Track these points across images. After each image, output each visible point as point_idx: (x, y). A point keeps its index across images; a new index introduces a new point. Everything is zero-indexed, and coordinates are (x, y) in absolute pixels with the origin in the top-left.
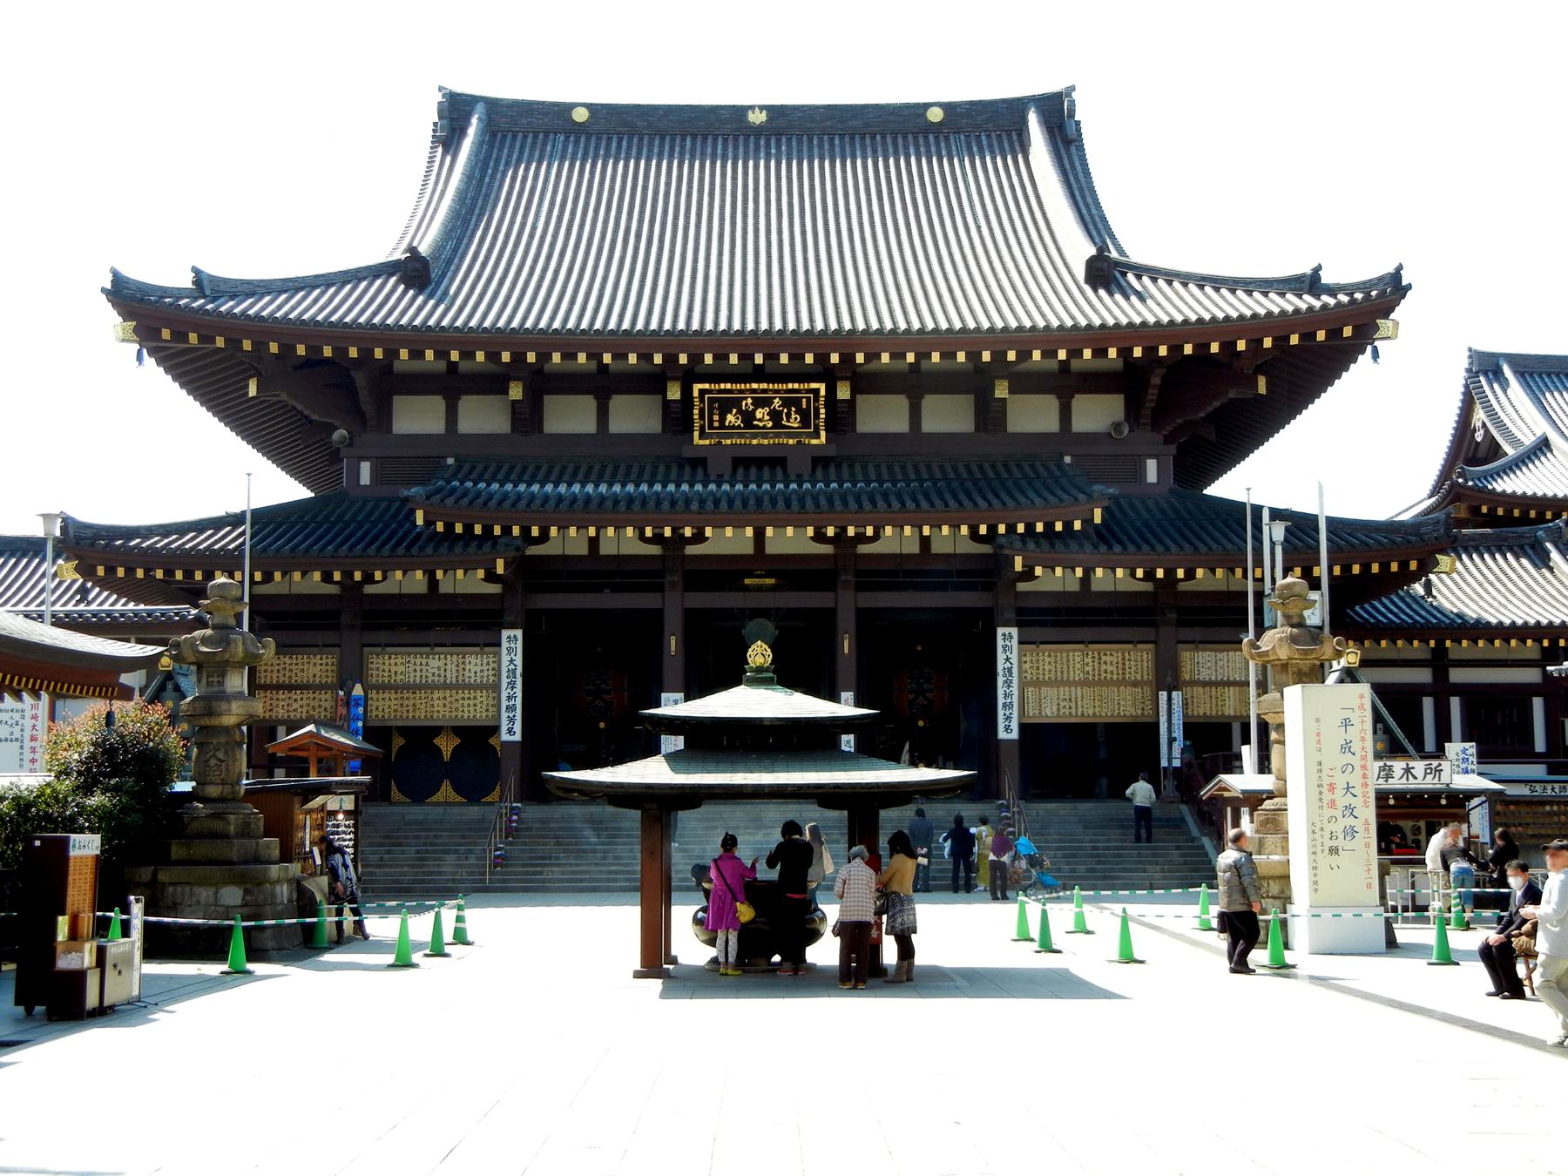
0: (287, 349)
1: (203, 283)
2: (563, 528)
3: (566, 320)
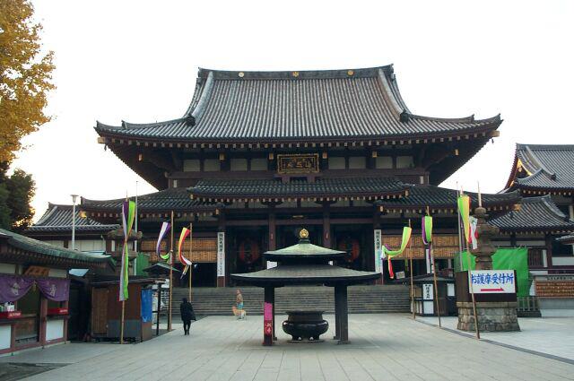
2: (286, 199)
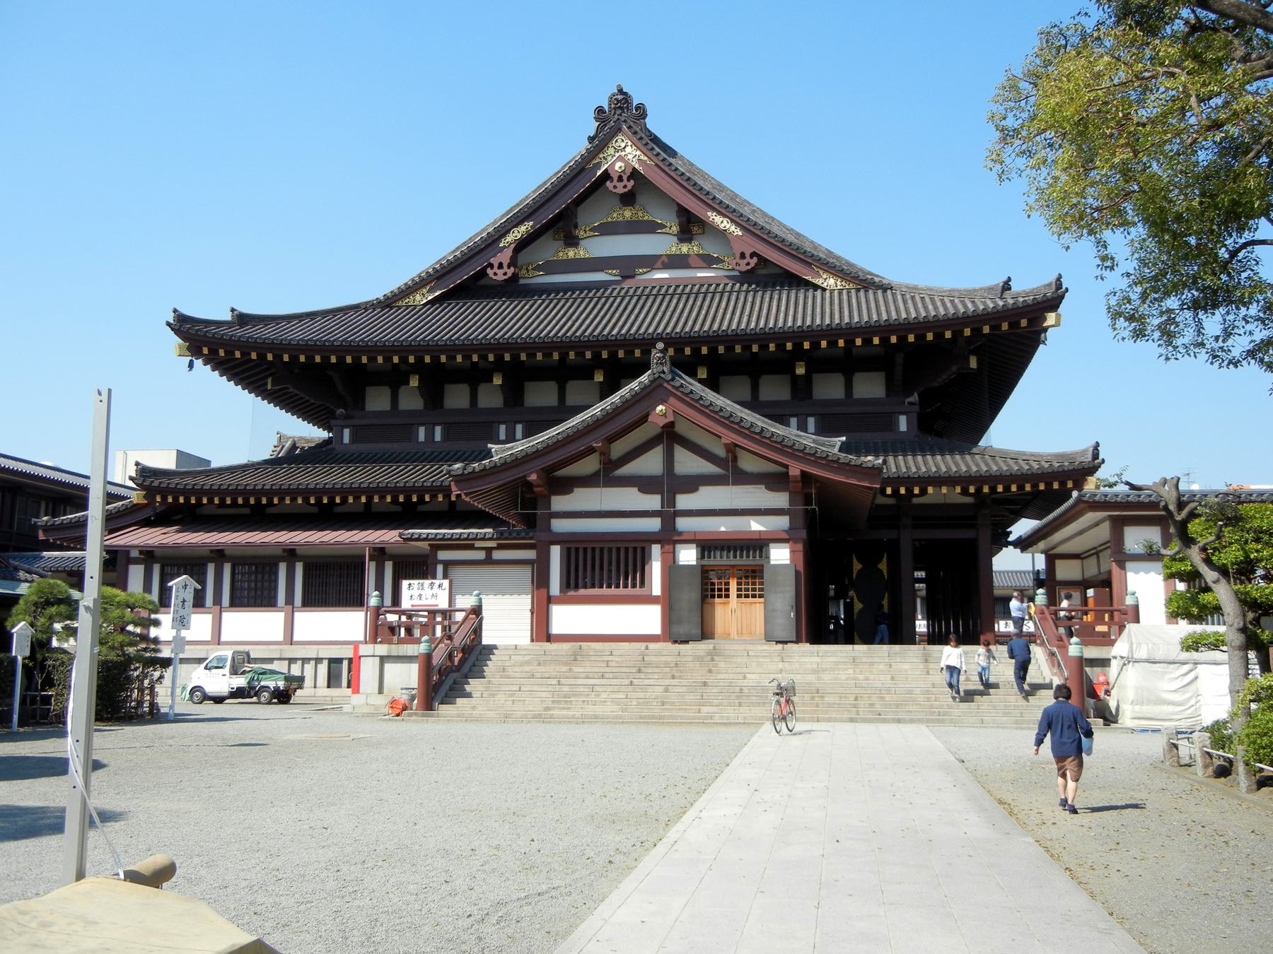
0: (294, 358)
1: (243, 319)
3: (739, 323)
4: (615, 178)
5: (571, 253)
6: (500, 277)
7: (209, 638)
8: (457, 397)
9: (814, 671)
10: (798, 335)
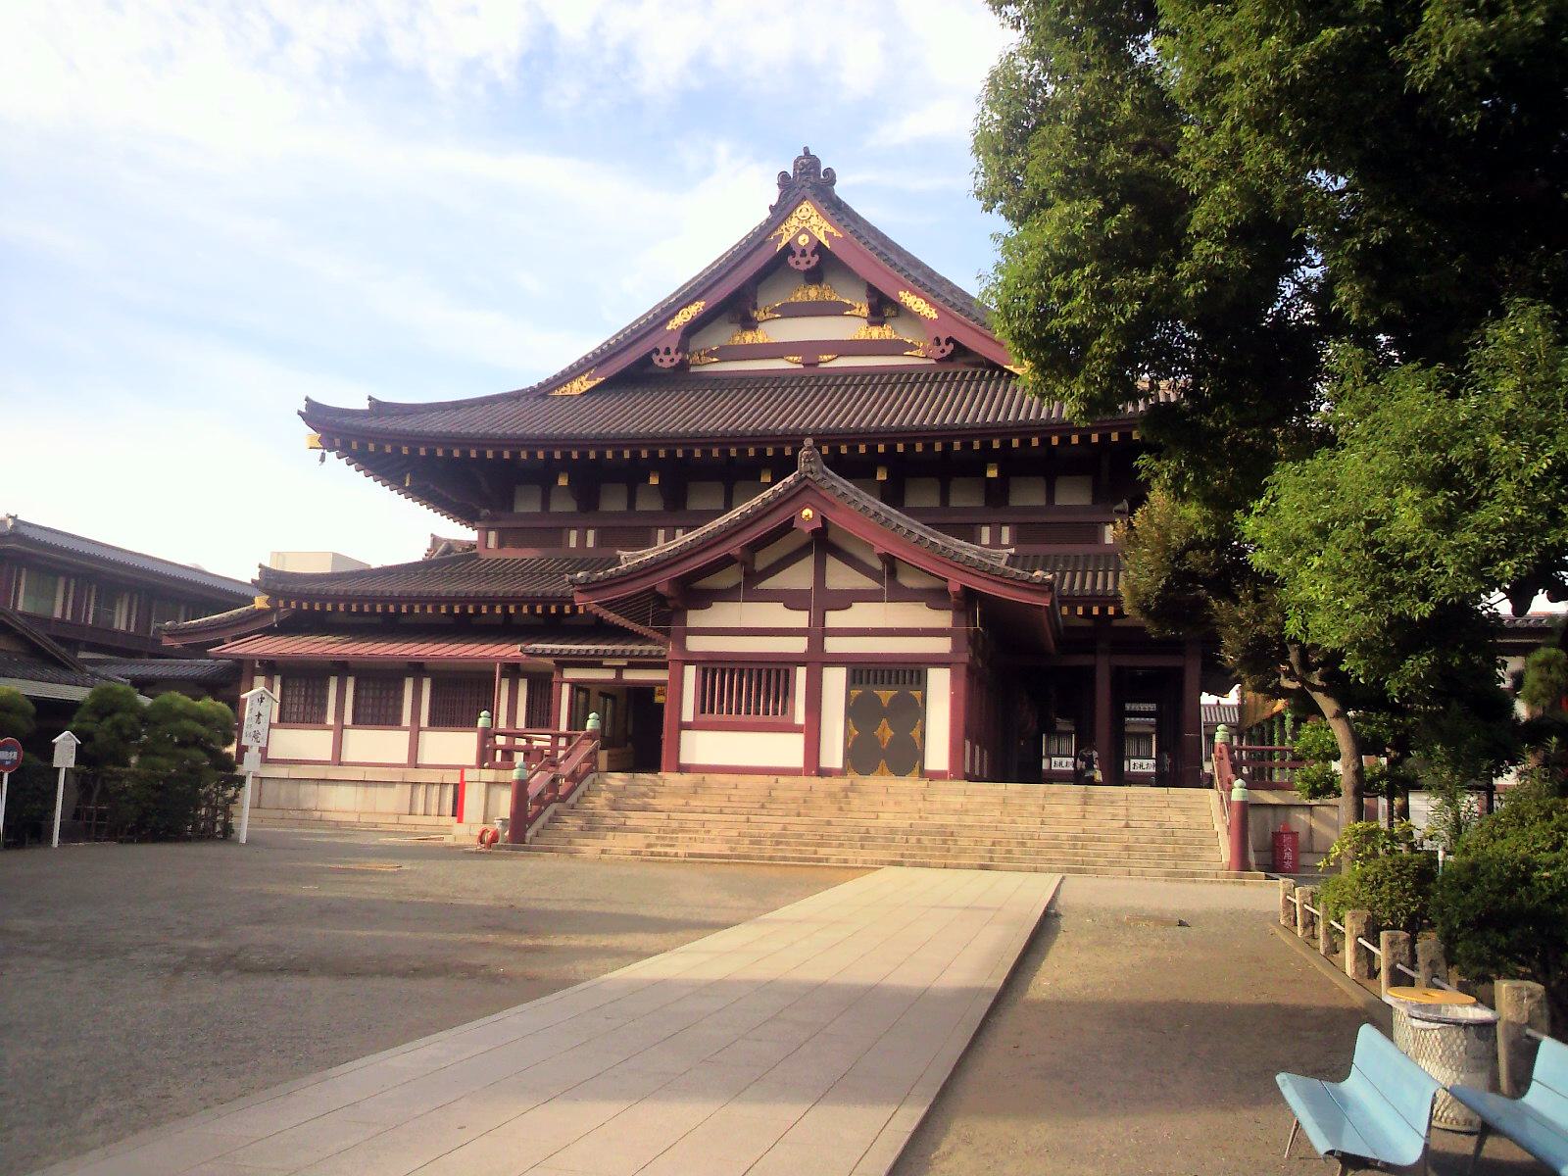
1: (378, 408)
3: (1007, 414)
4: (798, 253)
5: (749, 338)
6: (667, 364)
7: (406, 762)
8: (613, 502)
9: (956, 812)
10: (986, 432)
